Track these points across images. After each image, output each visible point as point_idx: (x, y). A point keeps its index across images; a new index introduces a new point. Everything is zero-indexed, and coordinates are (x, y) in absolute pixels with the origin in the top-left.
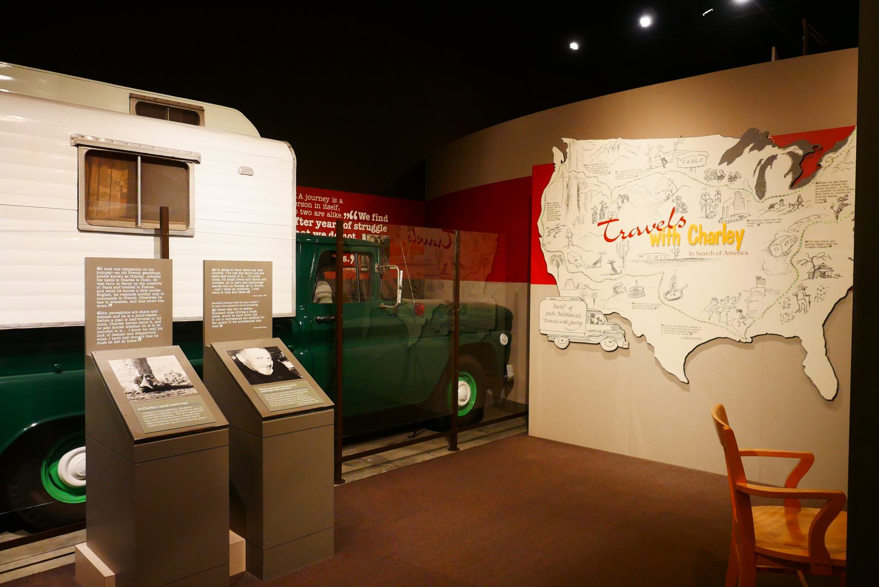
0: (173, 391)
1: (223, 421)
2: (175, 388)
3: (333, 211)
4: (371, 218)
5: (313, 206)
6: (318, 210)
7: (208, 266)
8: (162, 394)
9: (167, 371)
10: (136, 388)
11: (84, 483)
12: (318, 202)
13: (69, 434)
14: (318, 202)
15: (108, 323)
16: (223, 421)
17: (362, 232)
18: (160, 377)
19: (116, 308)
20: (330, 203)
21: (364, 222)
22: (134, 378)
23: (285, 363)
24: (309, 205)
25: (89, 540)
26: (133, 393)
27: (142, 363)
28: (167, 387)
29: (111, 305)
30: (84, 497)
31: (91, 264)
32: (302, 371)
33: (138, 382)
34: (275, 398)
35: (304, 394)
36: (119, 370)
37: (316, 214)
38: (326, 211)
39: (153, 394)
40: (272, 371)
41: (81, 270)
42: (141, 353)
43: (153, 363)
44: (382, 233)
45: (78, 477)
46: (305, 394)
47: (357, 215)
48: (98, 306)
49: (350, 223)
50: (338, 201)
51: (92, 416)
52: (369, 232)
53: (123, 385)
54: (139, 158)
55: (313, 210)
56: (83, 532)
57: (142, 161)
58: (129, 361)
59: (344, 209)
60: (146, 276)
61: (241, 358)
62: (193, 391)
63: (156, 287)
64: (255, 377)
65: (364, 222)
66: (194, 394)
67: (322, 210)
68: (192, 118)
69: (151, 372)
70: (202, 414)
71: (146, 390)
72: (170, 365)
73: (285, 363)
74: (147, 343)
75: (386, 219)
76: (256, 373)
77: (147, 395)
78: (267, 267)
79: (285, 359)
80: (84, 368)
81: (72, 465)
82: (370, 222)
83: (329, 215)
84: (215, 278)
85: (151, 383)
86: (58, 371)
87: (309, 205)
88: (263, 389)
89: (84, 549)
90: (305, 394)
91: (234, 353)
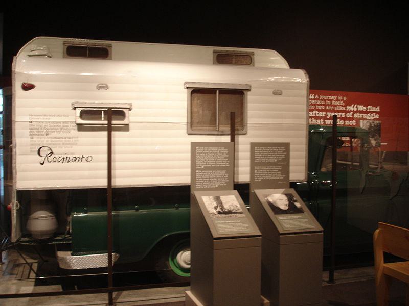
0: (232, 214)
1: (258, 233)
2: (234, 213)
3: (339, 105)
4: (367, 109)
5: (326, 103)
6: (329, 105)
7: (253, 145)
8: (227, 215)
9: (231, 204)
10: (215, 211)
11: (189, 266)
12: (329, 100)
13: (182, 242)
14: (329, 100)
15: (201, 177)
16: (258, 233)
17: (360, 119)
18: (227, 207)
19: (206, 169)
20: (337, 100)
21: (361, 112)
22: (214, 206)
23: (296, 203)
24: (323, 102)
25: (192, 290)
26: (213, 214)
27: (218, 199)
28: (230, 212)
29: (203, 167)
30: (189, 274)
31: (194, 145)
32: (306, 209)
33: (216, 208)
34: (287, 223)
35: (302, 223)
36: (207, 202)
37: (327, 108)
38: (334, 106)
39: (223, 215)
40: (287, 208)
41: (189, 147)
42: (217, 193)
43: (223, 198)
44: (375, 119)
45: (185, 262)
46: (306, 222)
47: (357, 107)
48: (197, 168)
49: (351, 113)
50: (343, 98)
51: (194, 230)
52: (366, 119)
53: (209, 209)
54: (218, 91)
55: (325, 105)
56: (189, 287)
57: (219, 94)
58: (211, 197)
59: (347, 103)
60: (220, 151)
61: (271, 200)
62: (243, 215)
63: (226, 158)
64: (277, 210)
65: (361, 112)
66: (243, 217)
67: (331, 105)
68: (247, 61)
69: (222, 204)
70: (247, 228)
71: (220, 213)
72: (232, 200)
73: (296, 203)
74: (220, 188)
75: (378, 109)
76: (278, 208)
77: (220, 216)
78: (286, 146)
79: (296, 201)
80: (189, 207)
81: (184, 257)
82: (366, 112)
83: (336, 108)
84: (256, 152)
85: (222, 209)
86: (177, 208)
87: (323, 102)
88: (281, 217)
89: (189, 293)
90: (306, 222)
91: (266, 196)
